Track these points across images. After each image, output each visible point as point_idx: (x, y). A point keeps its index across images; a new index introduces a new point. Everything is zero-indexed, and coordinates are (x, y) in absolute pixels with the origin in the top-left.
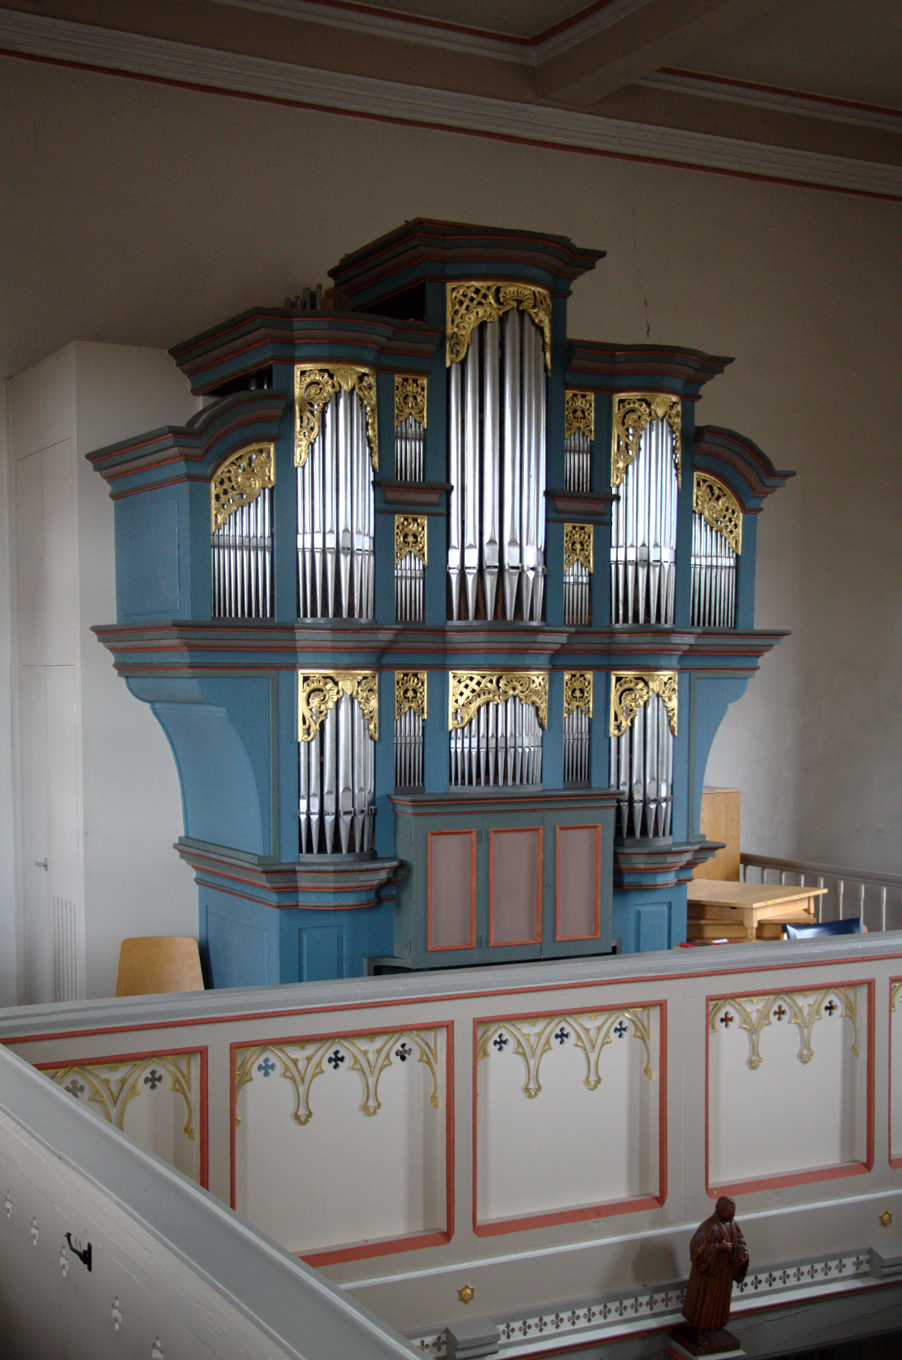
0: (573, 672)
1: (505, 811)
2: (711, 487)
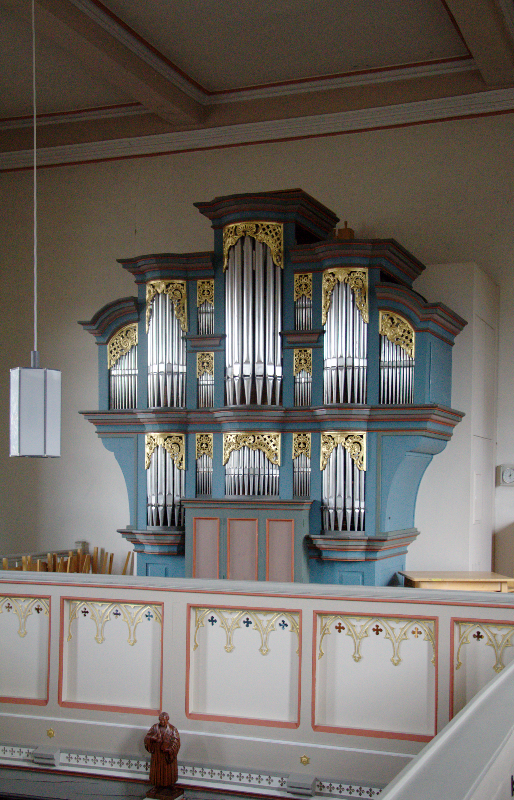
0: (299, 433)
1: (200, 508)
2: (392, 319)
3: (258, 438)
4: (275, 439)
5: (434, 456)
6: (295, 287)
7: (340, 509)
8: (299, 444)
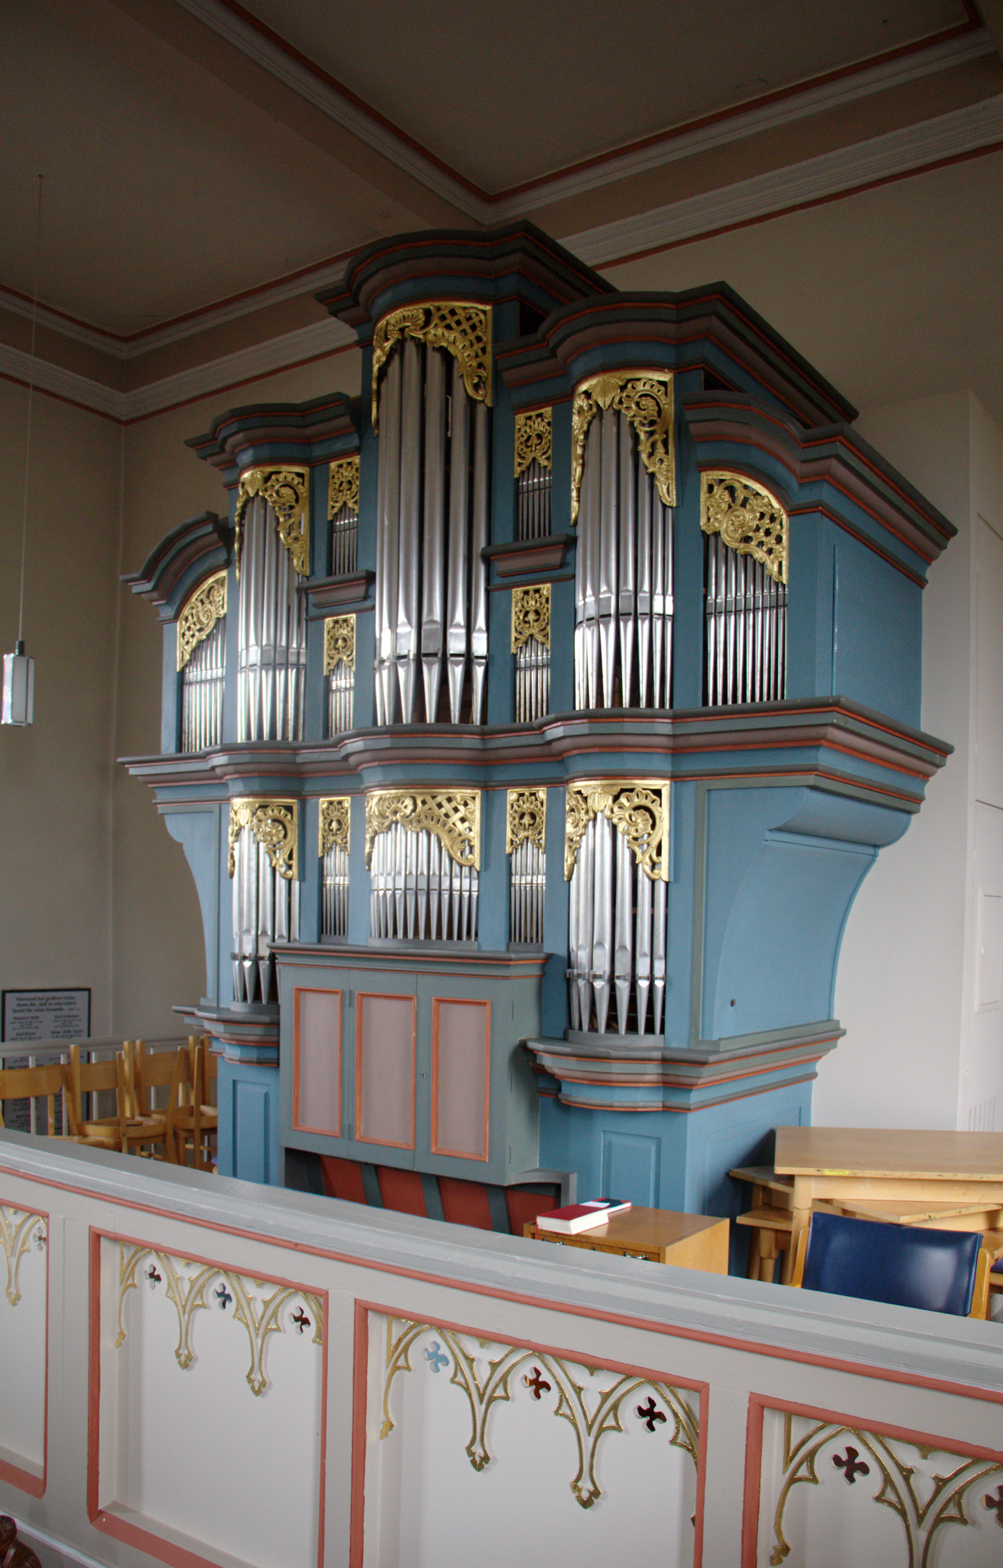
0: (521, 790)
3: (424, 802)
4: (466, 804)
5: (882, 852)
6: (517, 444)
7: (600, 977)
8: (522, 816)
